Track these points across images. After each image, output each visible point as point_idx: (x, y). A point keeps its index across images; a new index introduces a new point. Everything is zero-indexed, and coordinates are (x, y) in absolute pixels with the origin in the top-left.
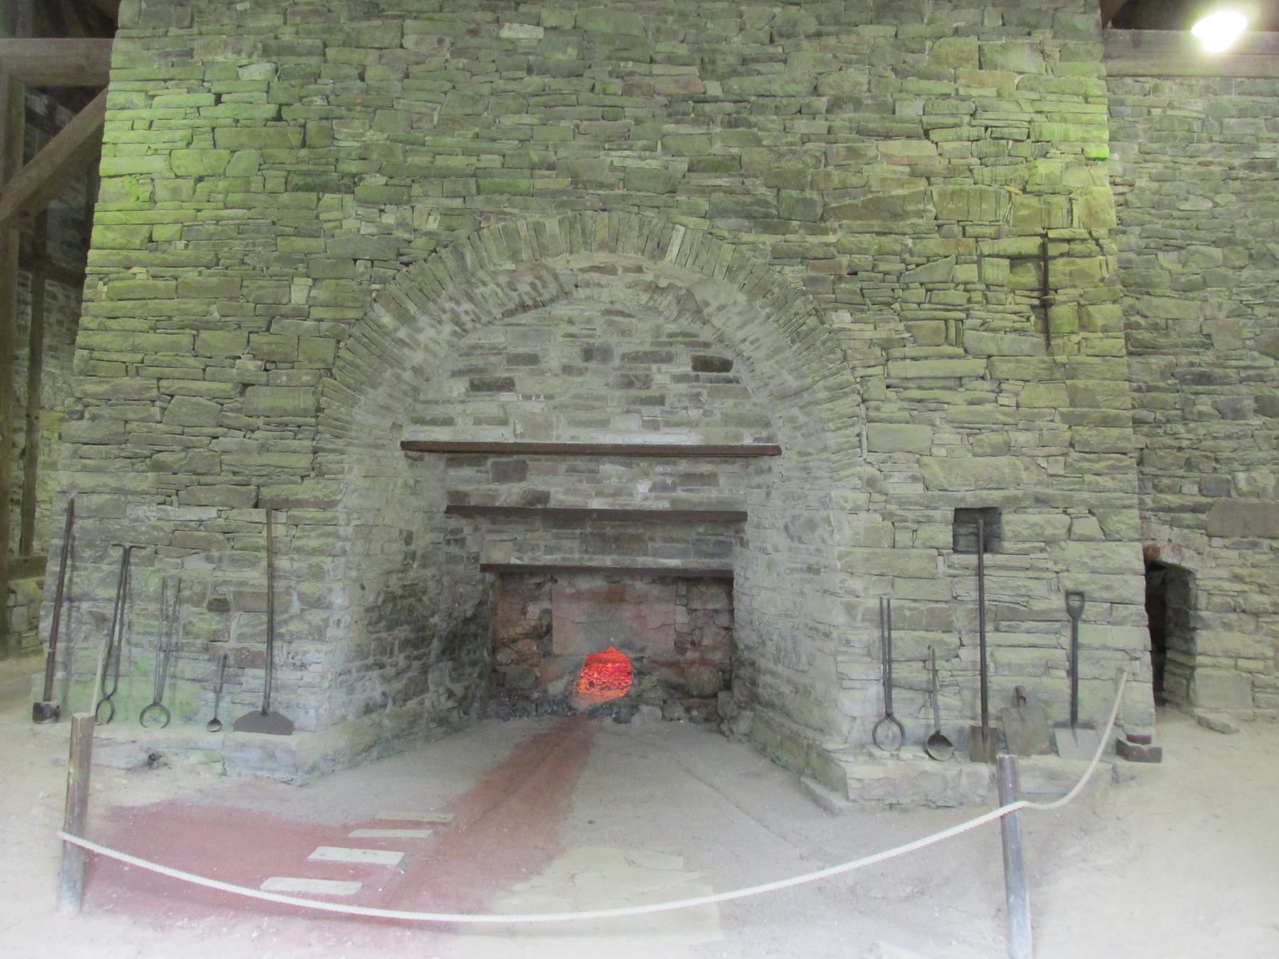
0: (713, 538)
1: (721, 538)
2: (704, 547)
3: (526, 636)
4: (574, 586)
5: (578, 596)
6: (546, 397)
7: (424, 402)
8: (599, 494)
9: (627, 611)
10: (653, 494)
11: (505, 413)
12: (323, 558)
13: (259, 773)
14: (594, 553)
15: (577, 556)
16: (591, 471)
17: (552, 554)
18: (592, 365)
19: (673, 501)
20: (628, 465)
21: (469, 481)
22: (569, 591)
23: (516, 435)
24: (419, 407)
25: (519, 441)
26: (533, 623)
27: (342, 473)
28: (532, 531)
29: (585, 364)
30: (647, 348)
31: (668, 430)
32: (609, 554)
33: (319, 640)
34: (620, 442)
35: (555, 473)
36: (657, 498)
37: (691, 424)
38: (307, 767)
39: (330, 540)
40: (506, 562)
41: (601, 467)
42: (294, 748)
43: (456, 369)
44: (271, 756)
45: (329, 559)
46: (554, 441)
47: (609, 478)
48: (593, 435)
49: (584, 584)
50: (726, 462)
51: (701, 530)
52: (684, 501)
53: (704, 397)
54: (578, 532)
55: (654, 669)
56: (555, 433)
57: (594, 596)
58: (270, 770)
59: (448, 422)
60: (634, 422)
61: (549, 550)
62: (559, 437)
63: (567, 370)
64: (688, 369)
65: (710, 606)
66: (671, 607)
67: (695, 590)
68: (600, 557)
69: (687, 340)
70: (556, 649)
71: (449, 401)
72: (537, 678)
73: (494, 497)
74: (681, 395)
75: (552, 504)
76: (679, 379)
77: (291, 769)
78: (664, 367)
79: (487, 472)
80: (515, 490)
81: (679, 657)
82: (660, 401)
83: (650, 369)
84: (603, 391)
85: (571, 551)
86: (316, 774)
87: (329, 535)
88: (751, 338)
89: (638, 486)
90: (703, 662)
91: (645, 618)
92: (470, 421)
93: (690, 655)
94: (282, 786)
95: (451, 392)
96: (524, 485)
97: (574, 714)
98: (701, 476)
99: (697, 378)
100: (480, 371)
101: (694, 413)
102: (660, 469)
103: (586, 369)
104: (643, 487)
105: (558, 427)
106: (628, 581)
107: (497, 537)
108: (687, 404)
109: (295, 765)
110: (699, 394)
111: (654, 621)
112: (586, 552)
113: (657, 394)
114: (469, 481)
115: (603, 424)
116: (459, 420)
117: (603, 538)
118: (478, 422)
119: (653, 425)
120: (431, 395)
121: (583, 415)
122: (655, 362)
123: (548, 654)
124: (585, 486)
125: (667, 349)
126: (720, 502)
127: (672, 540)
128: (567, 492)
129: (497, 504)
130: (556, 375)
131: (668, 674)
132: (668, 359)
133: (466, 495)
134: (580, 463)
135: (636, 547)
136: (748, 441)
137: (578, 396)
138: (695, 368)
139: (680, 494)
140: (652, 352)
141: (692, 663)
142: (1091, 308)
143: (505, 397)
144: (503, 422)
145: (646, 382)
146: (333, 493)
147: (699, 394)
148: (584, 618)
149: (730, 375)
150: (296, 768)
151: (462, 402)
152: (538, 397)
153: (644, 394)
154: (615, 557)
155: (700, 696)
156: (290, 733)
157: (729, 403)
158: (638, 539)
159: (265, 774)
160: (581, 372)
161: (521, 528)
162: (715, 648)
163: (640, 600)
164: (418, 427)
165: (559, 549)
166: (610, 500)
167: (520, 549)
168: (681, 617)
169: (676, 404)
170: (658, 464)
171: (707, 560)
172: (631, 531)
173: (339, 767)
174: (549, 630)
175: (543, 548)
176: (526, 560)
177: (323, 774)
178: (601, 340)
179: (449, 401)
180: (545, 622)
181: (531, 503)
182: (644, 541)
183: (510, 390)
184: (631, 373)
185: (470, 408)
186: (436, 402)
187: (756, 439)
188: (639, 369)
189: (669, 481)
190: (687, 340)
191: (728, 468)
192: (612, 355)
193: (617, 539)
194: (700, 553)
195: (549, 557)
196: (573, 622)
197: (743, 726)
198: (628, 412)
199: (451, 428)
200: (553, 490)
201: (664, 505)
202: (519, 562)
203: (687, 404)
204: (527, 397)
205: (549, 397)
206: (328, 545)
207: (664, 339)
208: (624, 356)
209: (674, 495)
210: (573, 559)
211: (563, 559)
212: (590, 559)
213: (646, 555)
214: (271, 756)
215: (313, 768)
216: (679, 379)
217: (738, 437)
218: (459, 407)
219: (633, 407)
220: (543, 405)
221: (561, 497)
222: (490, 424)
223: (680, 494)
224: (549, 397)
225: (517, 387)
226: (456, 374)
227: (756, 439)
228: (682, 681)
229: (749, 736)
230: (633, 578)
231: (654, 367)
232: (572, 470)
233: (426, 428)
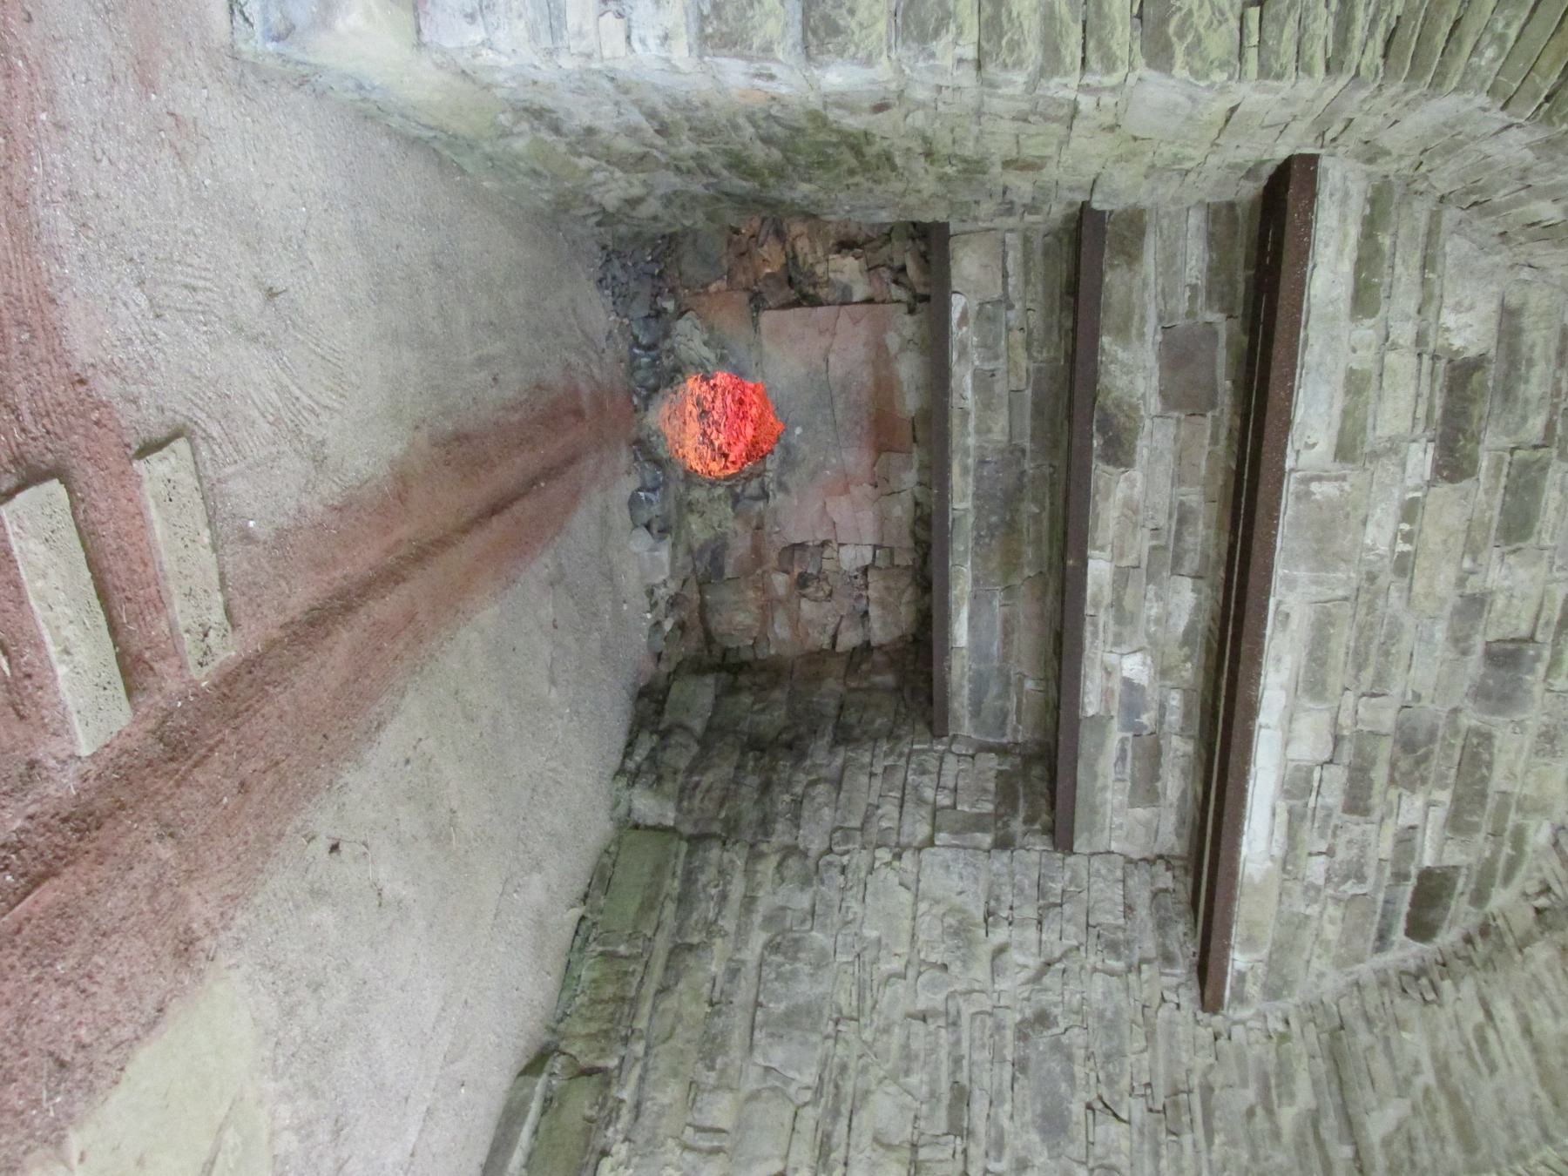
0: (1012, 704)
1: (1013, 718)
2: (994, 690)
3: (793, 258)
4: (902, 350)
5: (881, 357)
6: (1403, 555)
7: (1432, 233)
8: (1122, 577)
9: (856, 459)
10: (1117, 686)
11: (1375, 455)
12: (971, 33)
14: (979, 479)
15: (971, 441)
16: (1177, 560)
17: (975, 388)
18: (1474, 665)
19: (1100, 722)
20: (1187, 639)
21: (1170, 263)
22: (893, 341)
23: (1306, 481)
24: (1421, 210)
25: (1290, 486)
26: (820, 270)
27: (1264, 71)
28: (1028, 346)
29: (1479, 648)
30: (1498, 780)
31: (1282, 817)
32: (978, 509)
33: (704, 39)
34: (1262, 719)
35: (1178, 479)
36: (1107, 693)
37: (1288, 862)
39: (1033, 51)
40: (956, 284)
41: (1187, 583)
43: (1527, 321)
45: (970, 52)
46: (1279, 571)
47: (1159, 598)
48: (1288, 661)
49: (908, 369)
50: (1182, 822)
51: (1029, 684)
52: (1100, 746)
53: (1351, 888)
54: (1027, 444)
55: (747, 522)
56: (1302, 574)
57: (884, 387)
59: (1364, 299)
60: (1310, 744)
61: (984, 381)
62: (1291, 584)
63: (1474, 605)
64: (1428, 859)
65: (874, 611)
66: (870, 539)
67: (906, 580)
68: (970, 490)
69: (1501, 865)
70: (767, 318)
71: (1428, 300)
72: (705, 286)
73: (1122, 332)
74: (1363, 848)
75: (1101, 472)
76: (1406, 840)
78: (1438, 815)
79: (1191, 314)
80: (1140, 386)
81: (773, 556)
82: (1357, 802)
83: (1441, 782)
84: (1397, 689)
85: (982, 431)
87: (1052, 48)
88: (1491, 1035)
89: (1138, 657)
90: (768, 608)
91: (846, 491)
92: (1365, 360)
93: (780, 582)
95: (1458, 308)
96: (1155, 404)
97: (636, 410)
98: (1155, 777)
99: (1400, 876)
100: (1507, 392)
101: (1316, 869)
102: (1175, 700)
103: (1465, 652)
104: (1134, 667)
105: (1316, 582)
106: (917, 455)
107: (1014, 259)
108: (1341, 854)
109: (291, 29)
110: (1361, 879)
111: (840, 509)
112: (982, 462)
113: (1376, 800)
114: (1170, 263)
115: (1313, 684)
116: (1367, 332)
117: (1012, 498)
118: (1356, 383)
119: (1297, 786)
120: (1455, 247)
121: (1343, 638)
122: (1457, 799)
123: (757, 302)
124: (1142, 543)
125: (1486, 827)
126: (1093, 810)
127: (1007, 633)
128: (1130, 506)
129: (1105, 340)
130: (1461, 582)
131: (740, 546)
132: (1458, 823)
133: (1132, 255)
134: (1204, 537)
135: (992, 565)
136: (1239, 960)
137: (1393, 636)
138: (1426, 875)
139: (1116, 736)
140: (1483, 795)
141: (765, 589)
143: (1421, 458)
144: (1346, 450)
145: (1407, 778)
146: (1196, 47)
147: (1361, 879)
148: (837, 370)
149: (1399, 934)
151: (1420, 339)
152: (1408, 537)
153: (1380, 774)
154: (971, 519)
155: (703, 606)
157: (1332, 932)
158: (1011, 563)
160: (1460, 643)
161: (1035, 319)
162: (795, 622)
163: (881, 484)
164: (1357, 207)
165: (986, 405)
166: (1107, 596)
167: (986, 315)
168: (852, 557)
169: (1343, 838)
170: (1187, 703)
171: (966, 692)
172: (1029, 553)
174: (807, 300)
175: (988, 366)
176: (962, 333)
178: (1538, 689)
179: (1428, 300)
180: (823, 293)
181: (1106, 424)
182: (1006, 576)
183: (1437, 469)
184: (1437, 747)
185: (1402, 363)
186: (1427, 263)
187: (1241, 977)
188: (1444, 761)
189: (1146, 719)
190: (1501, 865)
191: (1169, 822)
192: (1496, 711)
193: (1011, 527)
194: (979, 685)
195: (968, 380)
196: (828, 350)
197: (648, 806)
198: (1337, 740)
199: (1344, 307)
200: (1137, 474)
201: (1091, 704)
202: (955, 314)
203: (1341, 854)
204: (1410, 511)
205: (1403, 566)
206: (1015, 46)
207: (1513, 818)
208: (1487, 738)
209: (1115, 724)
210: (965, 434)
211: (965, 414)
212: (965, 470)
213: (976, 581)
216: (1406, 840)
217: (1250, 943)
218: (1405, 333)
219: (1347, 751)
220: (1383, 548)
221: (1120, 491)
222: (1346, 414)
223: (1116, 736)
224: (1403, 566)
225: (1444, 488)
226: (1509, 320)
227: (1241, 977)
228: (729, 572)
229: (629, 826)
230: (924, 467)
231: (1444, 796)
232: (1184, 517)
233: (1354, 231)
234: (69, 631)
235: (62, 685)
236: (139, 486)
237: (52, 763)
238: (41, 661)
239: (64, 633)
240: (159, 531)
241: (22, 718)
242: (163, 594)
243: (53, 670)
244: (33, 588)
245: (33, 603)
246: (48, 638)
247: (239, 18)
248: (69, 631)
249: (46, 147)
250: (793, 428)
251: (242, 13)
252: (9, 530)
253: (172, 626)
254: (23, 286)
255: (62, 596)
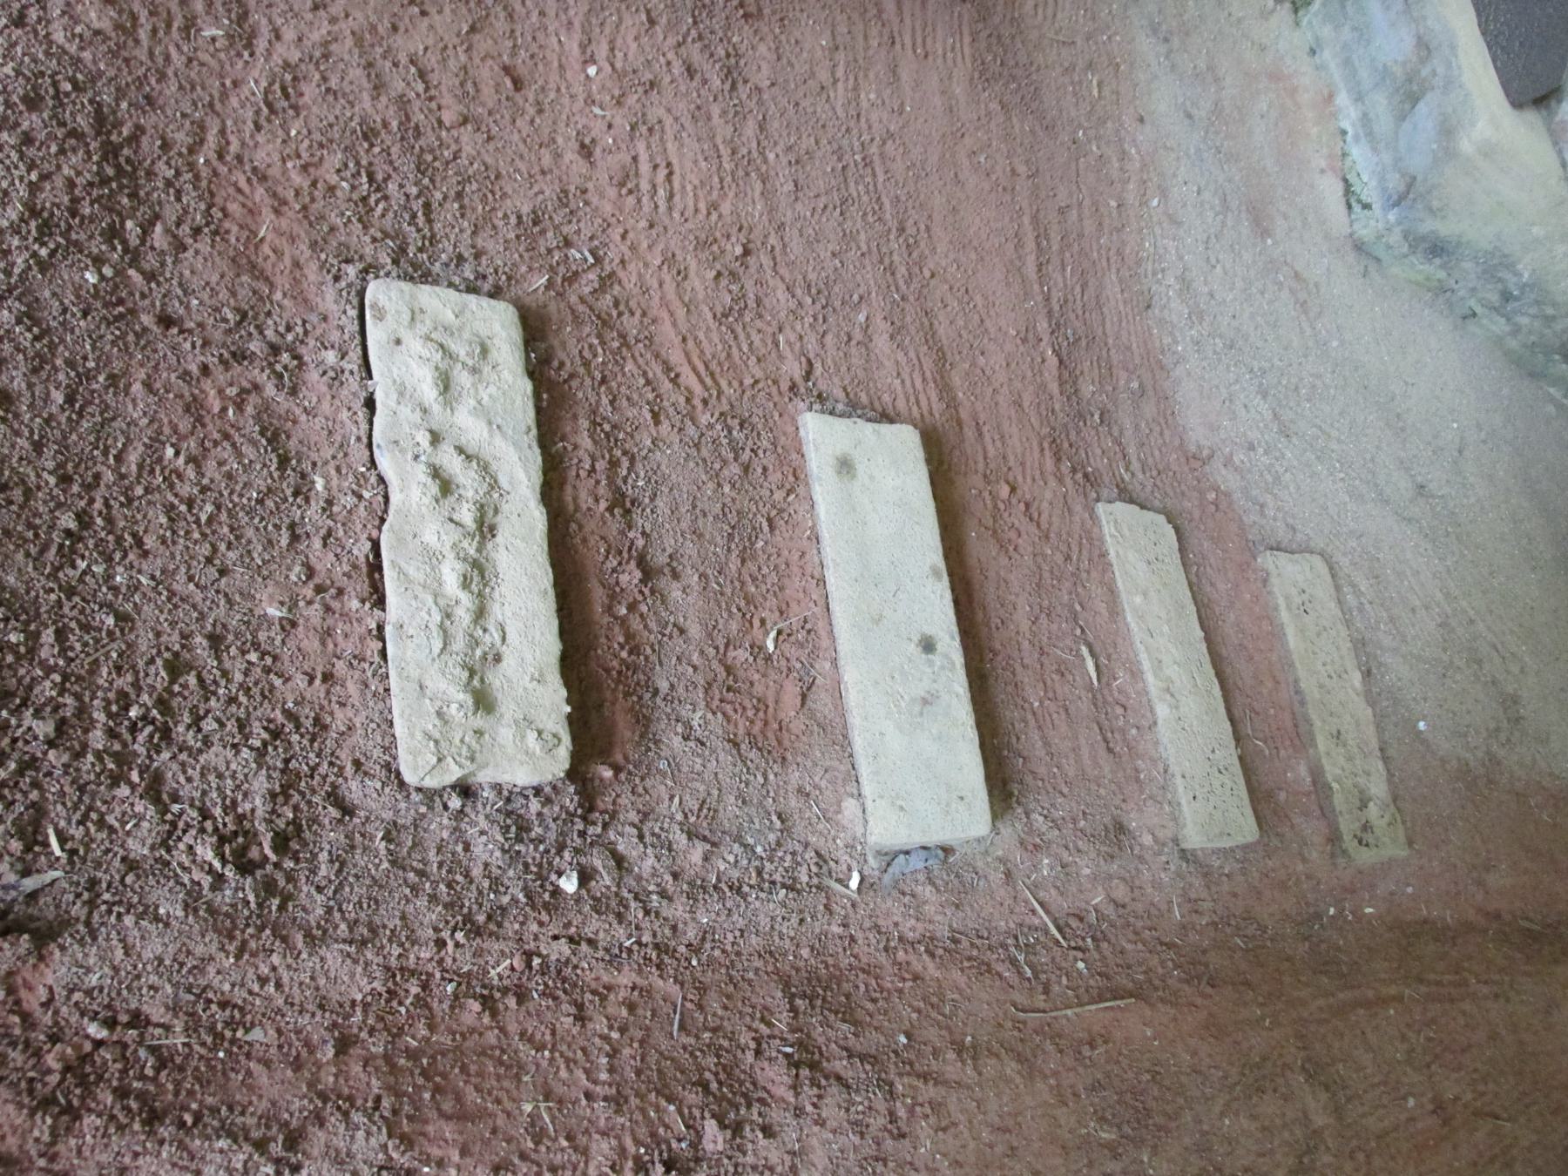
13: (1343, 99)
38: (1428, 226)
42: (1466, 146)
44: (1410, 94)
58: (1365, 119)
77: (1395, 183)
86: (1433, 270)
94: (1331, 190)
109: (1411, 182)
142: (1267, 560)
150: (1406, 195)
156: (1517, 103)
159: (1349, 118)
173: (1500, 326)
177: (1442, 290)
214: (1410, 94)
215: (1437, 249)
234: (1172, 671)
235: (1164, 732)
236: (1265, 581)
237: (1147, 840)
238: (1138, 693)
239: (1168, 672)
240: (1292, 640)
241: (1110, 750)
242: (1303, 728)
243: (1152, 710)
244: (1131, 602)
245: (1129, 619)
246: (1146, 665)
247: (1357, 208)
248: (1172, 671)
249: (1158, 231)
250: (421, 1099)
251: (1359, 201)
252: (1106, 530)
253: (1317, 773)
254: (1133, 338)
255: (1166, 629)
